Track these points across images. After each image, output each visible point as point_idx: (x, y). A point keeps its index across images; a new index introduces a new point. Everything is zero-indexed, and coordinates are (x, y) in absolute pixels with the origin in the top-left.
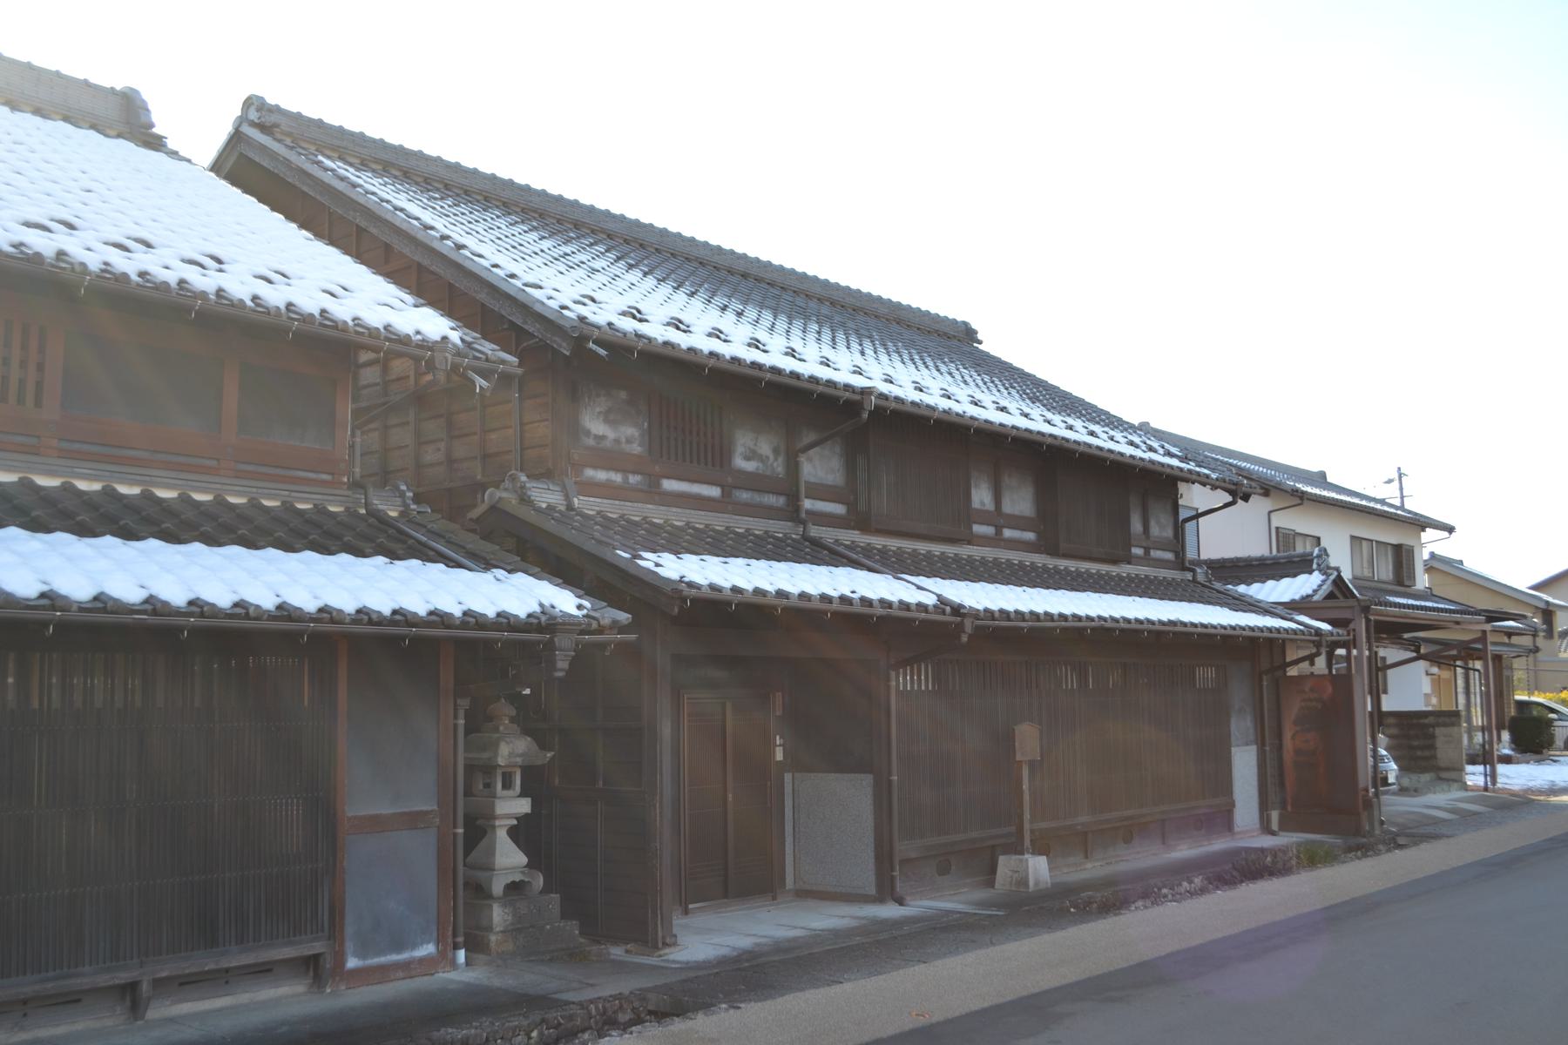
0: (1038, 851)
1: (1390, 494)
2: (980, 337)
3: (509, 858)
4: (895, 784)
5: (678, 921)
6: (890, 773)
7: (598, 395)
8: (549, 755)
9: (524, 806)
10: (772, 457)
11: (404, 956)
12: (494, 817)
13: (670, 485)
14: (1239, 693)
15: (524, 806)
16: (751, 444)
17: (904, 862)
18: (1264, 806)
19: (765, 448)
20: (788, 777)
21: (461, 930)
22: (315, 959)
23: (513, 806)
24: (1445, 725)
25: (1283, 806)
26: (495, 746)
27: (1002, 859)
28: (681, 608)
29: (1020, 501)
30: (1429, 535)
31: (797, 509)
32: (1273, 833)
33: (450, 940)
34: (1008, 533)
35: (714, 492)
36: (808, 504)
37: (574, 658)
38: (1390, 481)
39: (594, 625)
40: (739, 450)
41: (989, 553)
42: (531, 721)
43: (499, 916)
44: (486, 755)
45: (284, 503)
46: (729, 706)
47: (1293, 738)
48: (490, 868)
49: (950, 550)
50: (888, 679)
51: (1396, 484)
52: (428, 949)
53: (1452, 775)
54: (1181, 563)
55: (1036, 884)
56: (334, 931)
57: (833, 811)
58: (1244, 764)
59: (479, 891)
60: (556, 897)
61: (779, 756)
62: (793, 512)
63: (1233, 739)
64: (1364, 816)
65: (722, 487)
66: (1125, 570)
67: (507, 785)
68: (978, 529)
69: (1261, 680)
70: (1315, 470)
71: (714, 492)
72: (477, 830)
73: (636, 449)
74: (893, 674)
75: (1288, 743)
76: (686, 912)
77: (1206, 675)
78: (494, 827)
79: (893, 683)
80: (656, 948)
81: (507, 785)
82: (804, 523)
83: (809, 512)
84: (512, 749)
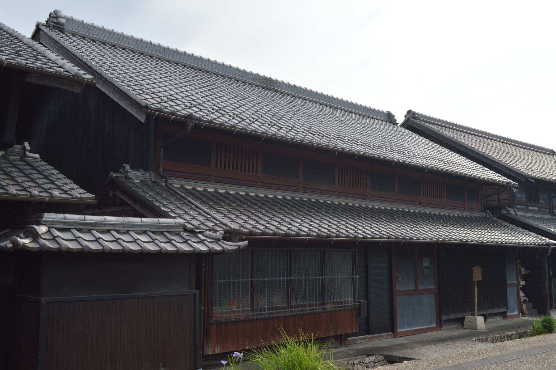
13: (530, 208)
35: (537, 209)
73: (525, 200)
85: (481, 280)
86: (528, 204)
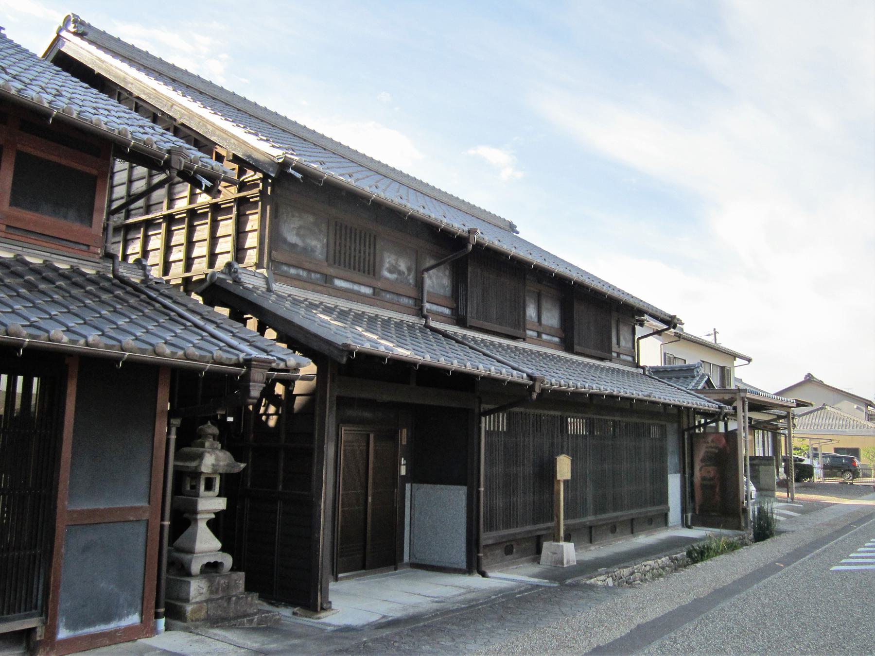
0: (567, 539)
1: (710, 340)
2: (517, 229)
3: (206, 544)
4: (482, 494)
5: (332, 586)
6: (479, 486)
7: (293, 216)
8: (243, 465)
9: (221, 504)
10: (406, 273)
11: (112, 626)
12: (195, 512)
13: (339, 283)
15: (221, 504)
16: (394, 262)
17: (486, 546)
18: (684, 510)
19: (403, 266)
20: (408, 486)
21: (162, 602)
22: (31, 631)
23: (212, 503)
24: (765, 465)
25: (694, 510)
26: (200, 457)
27: (546, 545)
28: (349, 359)
29: (552, 318)
30: (738, 362)
31: (421, 309)
32: (689, 527)
33: (153, 611)
34: (544, 337)
35: (367, 291)
36: (427, 306)
37: (264, 389)
38: (709, 335)
39: (282, 365)
41: (535, 348)
42: (230, 441)
43: (197, 588)
44: (194, 464)
45: (45, 261)
46: (372, 436)
47: (700, 470)
48: (191, 551)
49: (512, 343)
50: (480, 422)
51: (713, 337)
52: (134, 619)
53: (770, 493)
54: (638, 366)
55: (568, 562)
56: (46, 611)
57: (437, 511)
58: (674, 483)
59: (184, 571)
60: (242, 575)
61: (403, 471)
62: (420, 312)
64: (742, 517)
65: (374, 289)
66: (607, 364)
67: (209, 486)
68: (529, 333)
69: (684, 435)
71: (367, 291)
72: (183, 520)
74: (483, 419)
76: (336, 579)
78: (196, 520)
79: (483, 425)
80: (315, 611)
81: (209, 486)
82: (426, 317)
83: (429, 311)
84: (213, 460)
85: (569, 477)
86: (331, 271)
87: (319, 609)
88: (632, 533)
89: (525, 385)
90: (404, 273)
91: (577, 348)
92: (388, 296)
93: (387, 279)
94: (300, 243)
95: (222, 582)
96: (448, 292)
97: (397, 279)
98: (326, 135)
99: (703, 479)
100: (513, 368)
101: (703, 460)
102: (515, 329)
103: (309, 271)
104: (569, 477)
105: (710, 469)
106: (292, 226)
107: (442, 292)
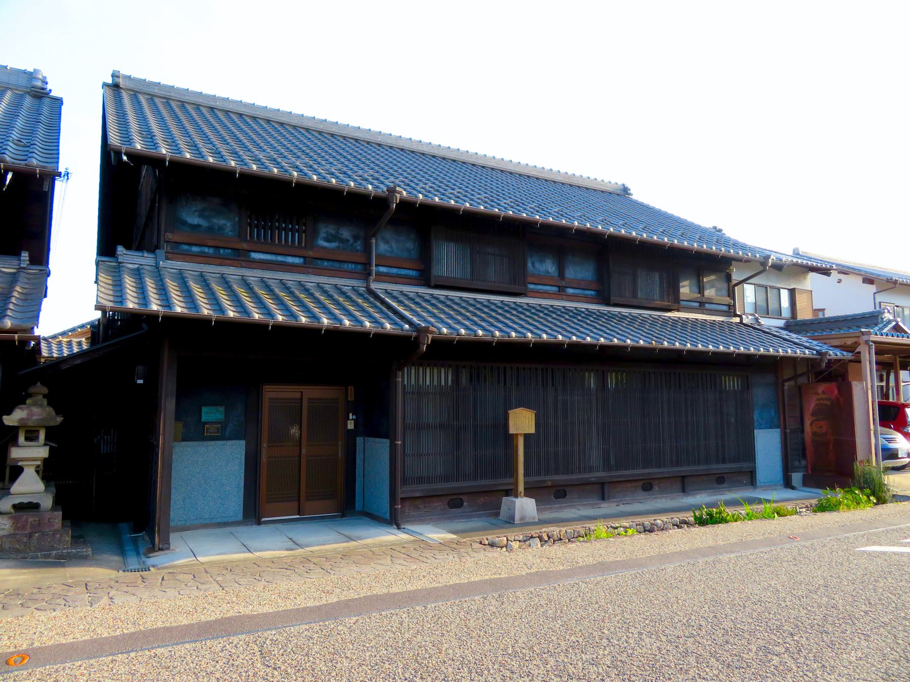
10: (351, 241)
14: (761, 394)
16: (333, 232)
20: (359, 440)
35: (297, 261)
40: (323, 235)
47: (811, 424)
63: (756, 424)
65: (559, 287)
70: (102, 91)
75: (304, 451)
77: (731, 383)
85: (532, 430)
87: (157, 549)
88: (684, 492)
89: (816, 359)
90: (348, 241)
91: (613, 299)
92: (326, 264)
93: (324, 248)
94: (204, 223)
95: (31, 519)
96: (415, 254)
97: (338, 247)
98: (638, 195)
99: (814, 434)
100: (806, 348)
101: (813, 415)
102: (516, 286)
103: (216, 247)
104: (532, 430)
105: (822, 423)
106: (194, 209)
107: (405, 255)
